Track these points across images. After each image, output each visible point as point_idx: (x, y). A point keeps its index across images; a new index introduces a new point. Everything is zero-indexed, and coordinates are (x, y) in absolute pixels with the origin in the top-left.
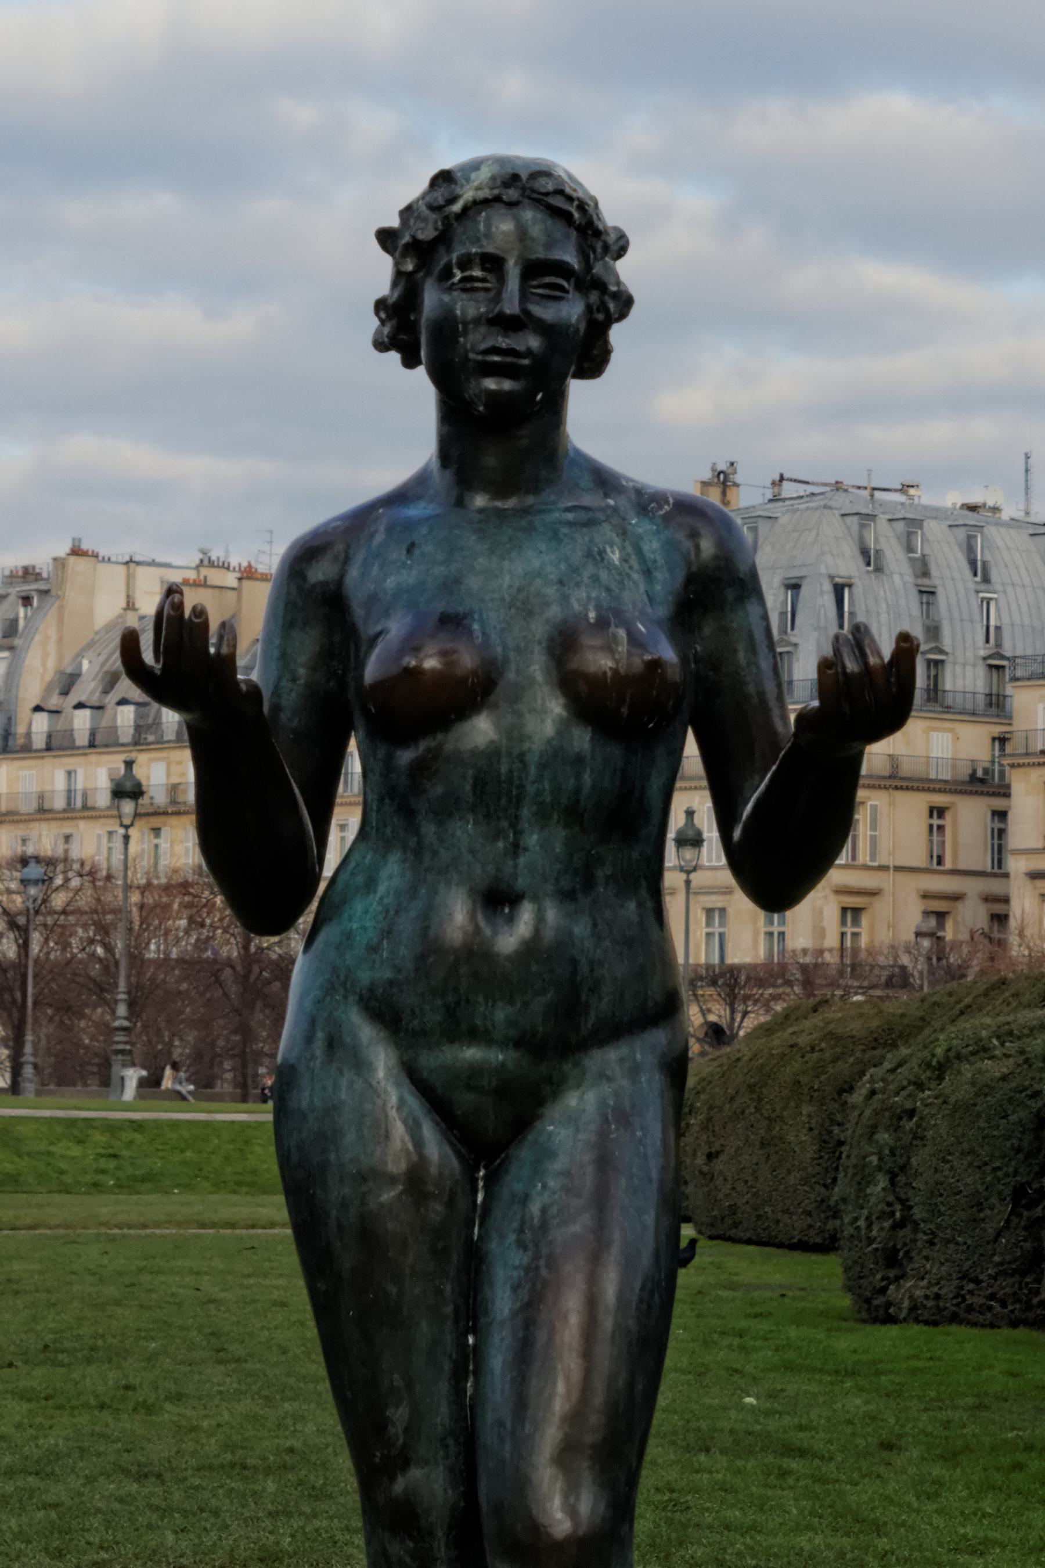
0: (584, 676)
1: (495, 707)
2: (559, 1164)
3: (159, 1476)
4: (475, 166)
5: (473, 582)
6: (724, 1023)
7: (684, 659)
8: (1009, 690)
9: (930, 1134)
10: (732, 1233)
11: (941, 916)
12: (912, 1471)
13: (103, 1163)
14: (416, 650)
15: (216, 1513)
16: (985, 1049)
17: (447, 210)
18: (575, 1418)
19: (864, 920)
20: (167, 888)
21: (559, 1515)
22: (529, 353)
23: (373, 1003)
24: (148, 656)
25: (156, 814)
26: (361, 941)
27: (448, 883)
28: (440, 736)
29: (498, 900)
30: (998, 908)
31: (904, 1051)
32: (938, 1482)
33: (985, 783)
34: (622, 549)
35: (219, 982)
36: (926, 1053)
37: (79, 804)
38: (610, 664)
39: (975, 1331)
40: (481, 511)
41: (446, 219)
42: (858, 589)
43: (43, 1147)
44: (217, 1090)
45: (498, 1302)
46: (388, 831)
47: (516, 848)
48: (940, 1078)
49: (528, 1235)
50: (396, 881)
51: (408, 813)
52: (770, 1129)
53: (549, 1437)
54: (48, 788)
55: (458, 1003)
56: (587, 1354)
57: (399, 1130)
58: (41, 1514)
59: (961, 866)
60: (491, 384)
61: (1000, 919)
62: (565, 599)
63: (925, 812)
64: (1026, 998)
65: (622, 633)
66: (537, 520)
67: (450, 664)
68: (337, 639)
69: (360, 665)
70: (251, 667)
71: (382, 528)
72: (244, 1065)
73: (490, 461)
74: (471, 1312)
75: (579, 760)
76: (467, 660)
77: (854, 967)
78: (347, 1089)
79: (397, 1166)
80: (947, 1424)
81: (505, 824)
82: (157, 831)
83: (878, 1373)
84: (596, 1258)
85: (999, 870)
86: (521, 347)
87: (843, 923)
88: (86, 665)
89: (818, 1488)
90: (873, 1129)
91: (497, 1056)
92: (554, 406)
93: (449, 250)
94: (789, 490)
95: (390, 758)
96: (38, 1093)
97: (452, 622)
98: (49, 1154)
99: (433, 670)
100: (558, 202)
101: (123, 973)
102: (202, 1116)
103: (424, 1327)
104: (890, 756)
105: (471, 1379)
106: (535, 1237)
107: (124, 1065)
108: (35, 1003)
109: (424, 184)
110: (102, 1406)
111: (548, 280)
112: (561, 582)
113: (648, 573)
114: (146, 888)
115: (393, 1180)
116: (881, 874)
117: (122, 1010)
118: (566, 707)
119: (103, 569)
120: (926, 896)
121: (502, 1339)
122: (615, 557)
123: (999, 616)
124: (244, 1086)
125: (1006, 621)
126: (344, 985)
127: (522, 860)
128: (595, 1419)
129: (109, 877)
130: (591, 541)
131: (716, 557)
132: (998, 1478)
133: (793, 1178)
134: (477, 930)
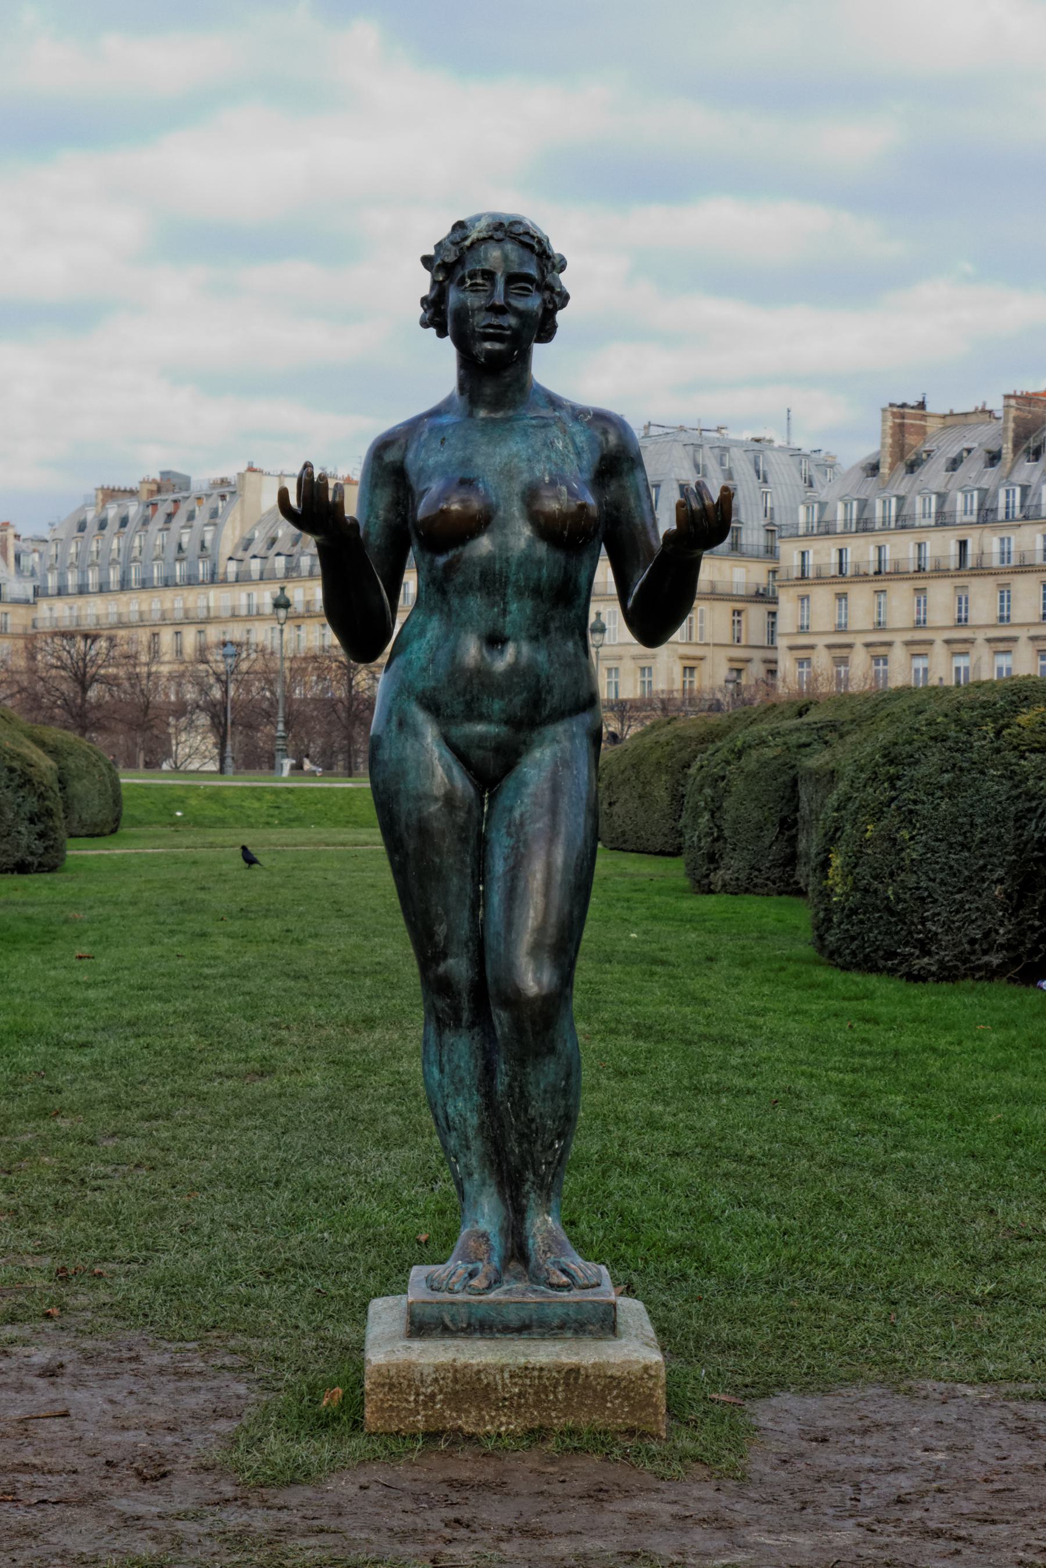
0: (543, 513)
1: (491, 531)
2: (531, 789)
3: (306, 977)
4: (478, 218)
5: (479, 460)
7: (600, 505)
8: (778, 543)
9: (733, 789)
10: (623, 846)
12: (724, 972)
14: (447, 499)
15: (338, 997)
16: (764, 742)
18: (541, 930)
19: (696, 673)
20: (305, 659)
21: (531, 984)
22: (510, 327)
24: (293, 501)
25: (298, 617)
26: (417, 665)
27: (466, 632)
29: (495, 641)
30: (772, 666)
31: (719, 744)
32: (738, 978)
33: (764, 597)
34: (564, 441)
35: (335, 711)
36: (731, 745)
37: (255, 612)
39: (758, 898)
40: (483, 419)
47: (504, 612)
48: (739, 758)
49: (513, 829)
50: (437, 631)
51: (443, 592)
52: (644, 788)
53: (526, 940)
56: (547, 894)
57: (439, 771)
58: (241, 998)
59: (751, 643)
60: (488, 345)
61: (772, 672)
62: (531, 469)
64: (788, 714)
65: (564, 489)
66: (515, 424)
67: (466, 507)
68: (401, 494)
69: (415, 509)
70: (352, 509)
72: (350, 756)
73: (488, 391)
74: (481, 872)
75: (540, 562)
76: (476, 505)
77: (690, 699)
78: (409, 750)
79: (439, 791)
80: (743, 948)
81: (498, 598)
82: (299, 627)
83: (704, 921)
84: (551, 841)
85: (772, 646)
86: (506, 325)
87: (684, 675)
88: (257, 534)
89: (672, 982)
92: (525, 357)
93: (463, 268)
94: (654, 431)
95: (432, 561)
96: (235, 773)
97: (467, 483)
98: (242, 807)
100: (526, 239)
101: (281, 706)
102: (326, 785)
104: (711, 582)
106: (517, 830)
108: (233, 723)
109: (449, 230)
110: (274, 941)
111: (523, 285)
112: (529, 460)
113: (579, 454)
114: (293, 659)
115: (436, 799)
116: (706, 648)
117: (281, 727)
118: (532, 531)
119: (266, 479)
120: (731, 660)
122: (560, 445)
124: (350, 769)
125: (776, 504)
127: (508, 619)
128: (551, 931)
129: (272, 653)
131: (618, 445)
132: (772, 975)
134: (483, 658)
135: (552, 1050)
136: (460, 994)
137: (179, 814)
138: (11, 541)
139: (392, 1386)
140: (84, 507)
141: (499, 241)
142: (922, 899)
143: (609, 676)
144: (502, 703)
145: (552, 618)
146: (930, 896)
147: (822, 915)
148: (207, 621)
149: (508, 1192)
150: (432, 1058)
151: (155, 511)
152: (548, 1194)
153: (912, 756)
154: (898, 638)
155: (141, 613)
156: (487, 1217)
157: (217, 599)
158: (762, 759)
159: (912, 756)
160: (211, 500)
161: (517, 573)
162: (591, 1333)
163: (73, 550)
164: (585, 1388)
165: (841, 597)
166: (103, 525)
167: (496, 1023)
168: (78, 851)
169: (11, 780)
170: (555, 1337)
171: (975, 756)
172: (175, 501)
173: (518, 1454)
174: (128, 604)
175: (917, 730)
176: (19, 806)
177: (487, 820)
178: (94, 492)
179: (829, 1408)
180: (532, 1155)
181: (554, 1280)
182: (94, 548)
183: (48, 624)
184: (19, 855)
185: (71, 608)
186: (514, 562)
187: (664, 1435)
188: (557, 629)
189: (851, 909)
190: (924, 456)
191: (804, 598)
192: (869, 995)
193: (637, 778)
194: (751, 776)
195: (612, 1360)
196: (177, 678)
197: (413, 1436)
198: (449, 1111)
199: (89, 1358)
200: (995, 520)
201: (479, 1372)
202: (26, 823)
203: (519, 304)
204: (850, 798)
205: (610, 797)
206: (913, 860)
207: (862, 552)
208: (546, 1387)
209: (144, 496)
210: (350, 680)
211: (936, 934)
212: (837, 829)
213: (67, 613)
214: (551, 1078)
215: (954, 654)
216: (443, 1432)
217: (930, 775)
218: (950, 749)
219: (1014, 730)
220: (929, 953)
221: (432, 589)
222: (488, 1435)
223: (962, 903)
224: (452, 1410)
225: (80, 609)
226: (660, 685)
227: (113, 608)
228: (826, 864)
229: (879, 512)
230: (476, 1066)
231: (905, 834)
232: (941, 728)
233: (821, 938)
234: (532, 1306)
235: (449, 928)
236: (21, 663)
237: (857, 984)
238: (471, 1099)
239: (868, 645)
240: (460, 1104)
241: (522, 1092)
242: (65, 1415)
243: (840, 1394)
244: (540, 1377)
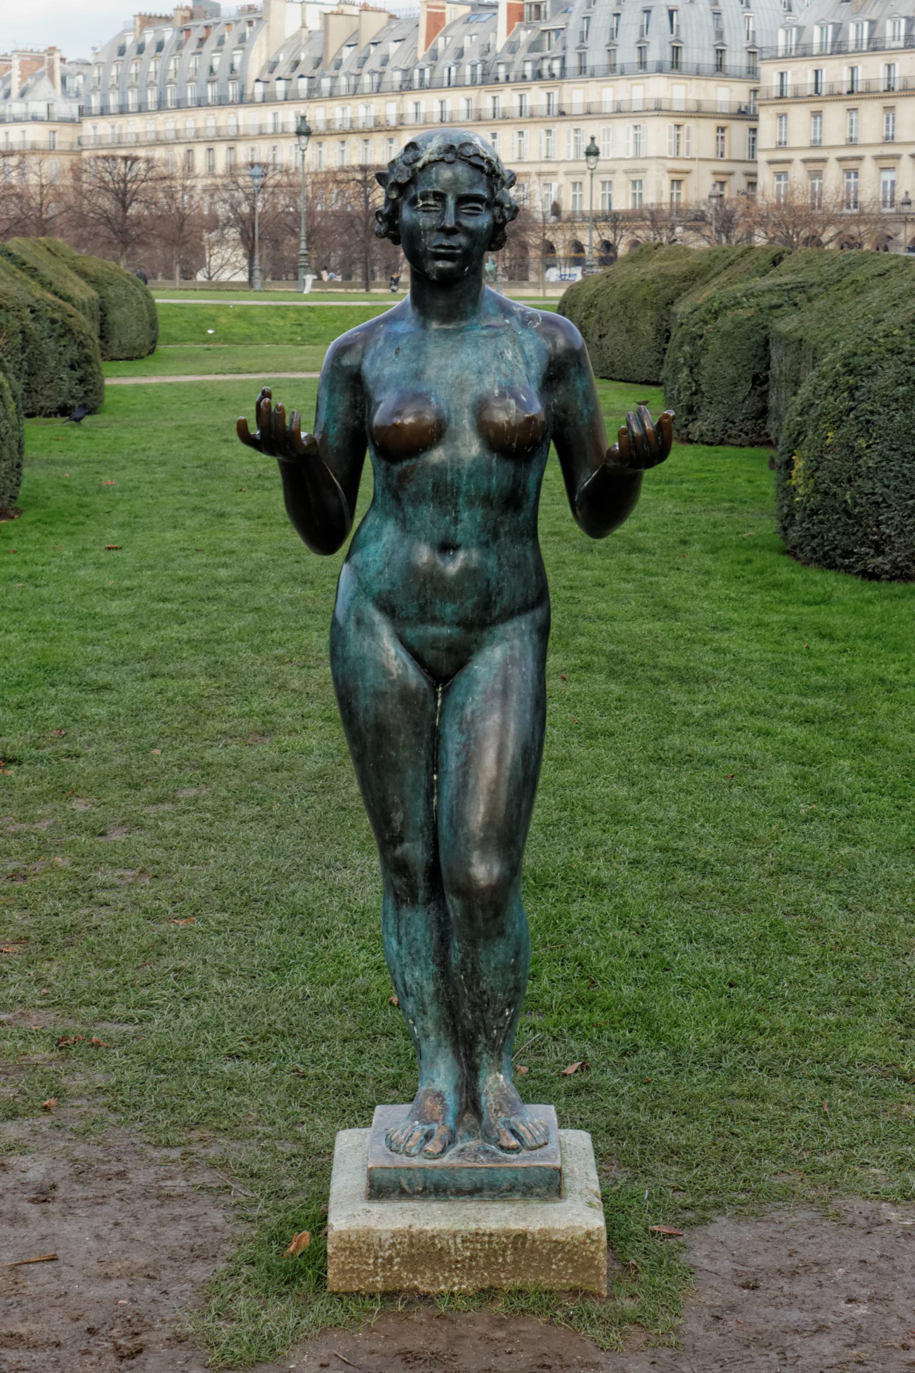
0: (492, 424)
5: (431, 373)
6: (611, 241)
8: (759, 65)
9: (710, 348)
10: (612, 375)
11: (722, 183)
13: (295, 329)
16: (739, 303)
19: (683, 186)
22: (460, 246)
25: (319, 135)
28: (414, 460)
29: (446, 547)
30: (752, 179)
33: (746, 114)
34: (514, 350)
37: (280, 130)
40: (436, 330)
41: (414, 170)
42: (681, 13)
43: (264, 320)
44: (354, 280)
46: (388, 507)
47: (456, 521)
48: (716, 318)
49: (464, 726)
51: (398, 499)
52: (631, 323)
54: (264, 122)
60: (440, 264)
61: (752, 185)
63: (715, 130)
68: (358, 398)
69: (371, 417)
71: (382, 337)
74: (435, 763)
76: (429, 417)
81: (450, 507)
82: (320, 144)
85: (753, 160)
87: (672, 188)
88: (281, 57)
90: (681, 344)
91: (446, 631)
92: (477, 272)
97: (420, 397)
98: (268, 324)
99: (410, 424)
103: (410, 772)
107: (305, 274)
108: (260, 238)
113: (527, 364)
116: (691, 162)
120: (715, 173)
122: (509, 355)
123: (754, 26)
126: (364, 591)
127: (459, 527)
133: (643, 348)
135: (501, 933)
136: (416, 875)
137: (210, 332)
138: (58, 64)
139: (352, 1250)
140: (124, 31)
141: (450, 163)
142: (877, 504)
143: (604, 188)
144: (453, 606)
145: (502, 523)
146: (884, 501)
147: (785, 510)
148: (236, 138)
149: (462, 1050)
150: (390, 930)
151: (188, 36)
152: (499, 1054)
153: (869, 368)
154: (869, 153)
155: (177, 131)
156: (442, 1076)
157: (247, 118)
158: (737, 320)
159: (869, 368)
160: (240, 25)
161: (468, 483)
162: (537, 1195)
163: (114, 73)
164: (532, 1252)
165: (817, 114)
166: (141, 49)
167: (450, 906)
168: (118, 380)
169: (53, 331)
170: (504, 1199)
172: (207, 27)
173: (469, 1315)
174: (165, 123)
175: (875, 341)
176: (61, 354)
178: (132, 19)
179: (761, 1238)
180: (484, 1021)
181: (505, 1143)
182: (133, 71)
183: (92, 141)
184: (62, 399)
185: (113, 127)
186: (464, 473)
187: (605, 1293)
188: (506, 533)
189: (812, 510)
191: (782, 116)
192: (826, 600)
193: (625, 313)
194: (727, 336)
195: (557, 1227)
196: (212, 190)
197: (372, 1297)
198: (407, 979)
199: (82, 1173)
201: (433, 1237)
202: (68, 369)
204: (812, 405)
205: (600, 330)
206: (869, 468)
207: (836, 72)
208: (495, 1251)
209: (178, 22)
210: (367, 197)
211: (890, 536)
212: (800, 433)
213: (109, 131)
214: (502, 957)
216: (400, 1291)
218: (905, 362)
220: (883, 553)
221: (388, 495)
222: (441, 1295)
224: (408, 1272)
225: (121, 127)
226: (650, 199)
227: (151, 127)
228: (789, 465)
229: (852, 36)
230: (431, 939)
231: (862, 442)
232: (897, 340)
234: (483, 1171)
235: (405, 814)
236: (68, 181)
237: (815, 583)
238: (427, 968)
239: (840, 160)
240: (417, 974)
241: (474, 969)
242: (53, 1259)
243: (773, 1220)
244: (490, 1242)
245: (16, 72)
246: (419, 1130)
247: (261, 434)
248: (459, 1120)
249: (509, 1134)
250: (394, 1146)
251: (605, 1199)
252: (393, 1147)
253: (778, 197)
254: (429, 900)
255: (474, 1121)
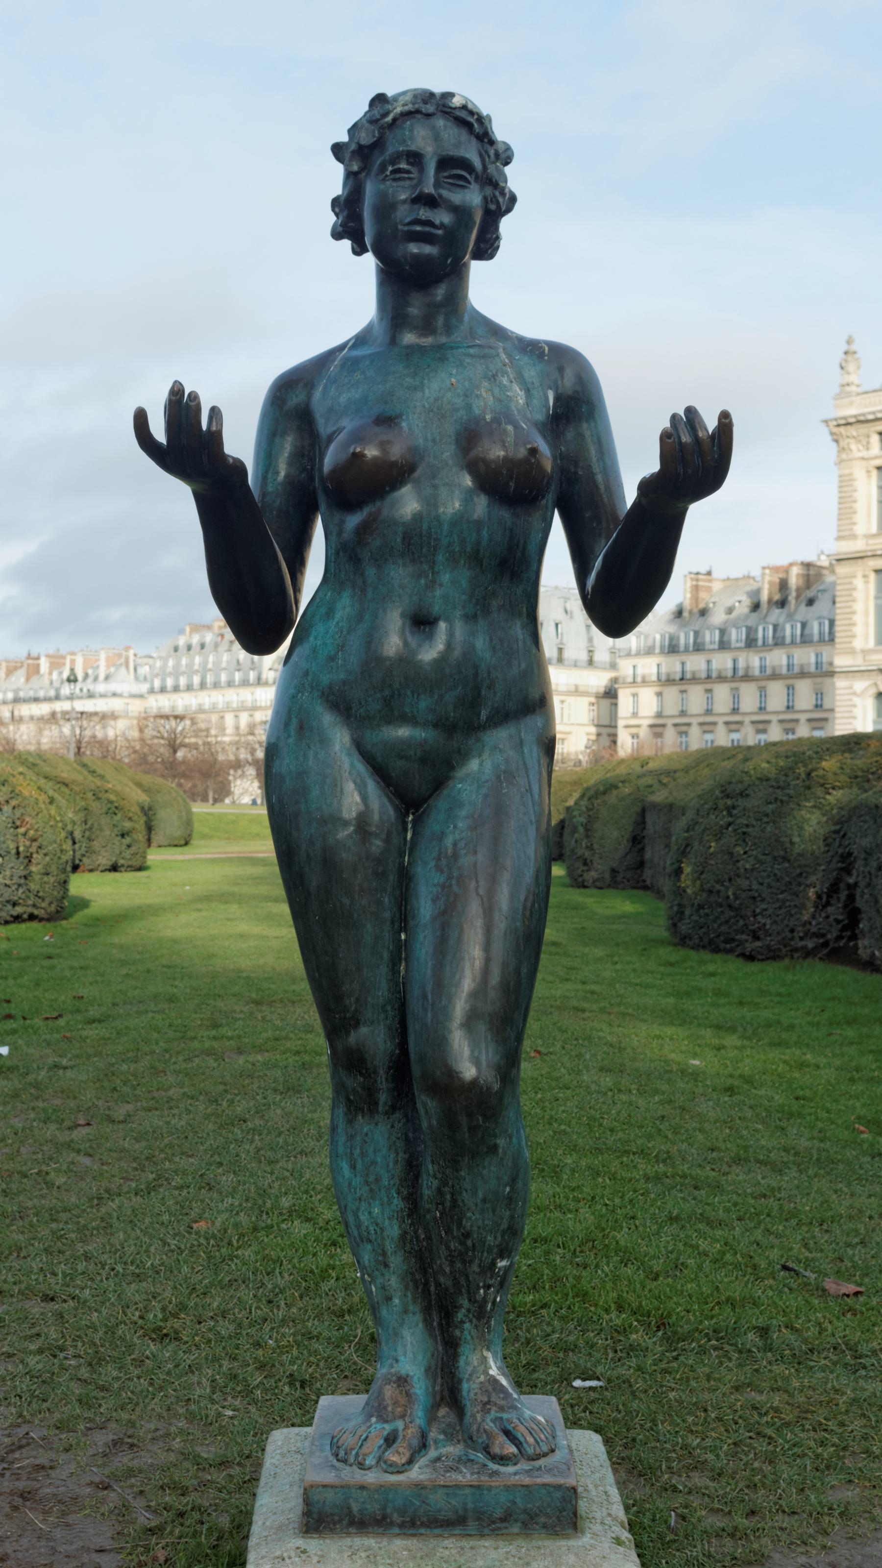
0: (484, 461)
4: (404, 93)
8: (618, 660)
17: (382, 122)
22: (442, 226)
23: (331, 698)
28: (378, 504)
29: (422, 622)
38: (502, 453)
40: (408, 347)
45: (422, 910)
46: (343, 575)
49: (444, 862)
51: (355, 560)
53: (460, 1008)
55: (392, 696)
56: (487, 948)
60: (414, 248)
74: (403, 917)
76: (396, 452)
81: (425, 567)
95: (342, 522)
99: (375, 458)
100: (463, 114)
105: (403, 964)
115: (346, 823)
121: (425, 937)
130: (487, 368)
138: (132, 658)
141: (428, 115)
142: (754, 898)
146: (759, 896)
147: (675, 908)
150: (341, 1150)
156: (410, 1355)
166: (189, 648)
167: (422, 1112)
171: (792, 792)
177: (411, 850)
180: (467, 1277)
181: (496, 1450)
190: (711, 605)
191: (635, 695)
196: (237, 745)
198: (362, 1218)
200: (756, 646)
203: (456, 197)
204: (697, 823)
212: (687, 845)
215: (731, 731)
217: (758, 806)
219: (821, 772)
220: (758, 939)
223: (784, 901)
228: (678, 872)
230: (396, 1162)
233: (675, 925)
236: (135, 734)
239: (675, 725)
241: (454, 1201)
245: (102, 663)
246: (379, 1429)
247: (168, 441)
248: (431, 1417)
249: (502, 1438)
250: (342, 1454)
251: (632, 1527)
252: (340, 1454)
253: (633, 749)
254: (394, 1108)
255: (452, 1418)
